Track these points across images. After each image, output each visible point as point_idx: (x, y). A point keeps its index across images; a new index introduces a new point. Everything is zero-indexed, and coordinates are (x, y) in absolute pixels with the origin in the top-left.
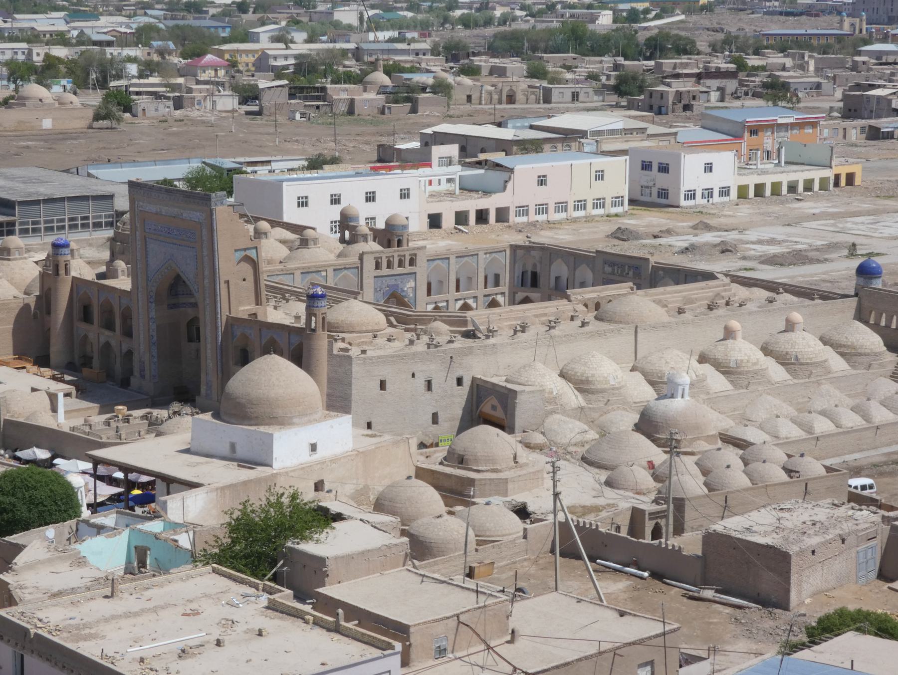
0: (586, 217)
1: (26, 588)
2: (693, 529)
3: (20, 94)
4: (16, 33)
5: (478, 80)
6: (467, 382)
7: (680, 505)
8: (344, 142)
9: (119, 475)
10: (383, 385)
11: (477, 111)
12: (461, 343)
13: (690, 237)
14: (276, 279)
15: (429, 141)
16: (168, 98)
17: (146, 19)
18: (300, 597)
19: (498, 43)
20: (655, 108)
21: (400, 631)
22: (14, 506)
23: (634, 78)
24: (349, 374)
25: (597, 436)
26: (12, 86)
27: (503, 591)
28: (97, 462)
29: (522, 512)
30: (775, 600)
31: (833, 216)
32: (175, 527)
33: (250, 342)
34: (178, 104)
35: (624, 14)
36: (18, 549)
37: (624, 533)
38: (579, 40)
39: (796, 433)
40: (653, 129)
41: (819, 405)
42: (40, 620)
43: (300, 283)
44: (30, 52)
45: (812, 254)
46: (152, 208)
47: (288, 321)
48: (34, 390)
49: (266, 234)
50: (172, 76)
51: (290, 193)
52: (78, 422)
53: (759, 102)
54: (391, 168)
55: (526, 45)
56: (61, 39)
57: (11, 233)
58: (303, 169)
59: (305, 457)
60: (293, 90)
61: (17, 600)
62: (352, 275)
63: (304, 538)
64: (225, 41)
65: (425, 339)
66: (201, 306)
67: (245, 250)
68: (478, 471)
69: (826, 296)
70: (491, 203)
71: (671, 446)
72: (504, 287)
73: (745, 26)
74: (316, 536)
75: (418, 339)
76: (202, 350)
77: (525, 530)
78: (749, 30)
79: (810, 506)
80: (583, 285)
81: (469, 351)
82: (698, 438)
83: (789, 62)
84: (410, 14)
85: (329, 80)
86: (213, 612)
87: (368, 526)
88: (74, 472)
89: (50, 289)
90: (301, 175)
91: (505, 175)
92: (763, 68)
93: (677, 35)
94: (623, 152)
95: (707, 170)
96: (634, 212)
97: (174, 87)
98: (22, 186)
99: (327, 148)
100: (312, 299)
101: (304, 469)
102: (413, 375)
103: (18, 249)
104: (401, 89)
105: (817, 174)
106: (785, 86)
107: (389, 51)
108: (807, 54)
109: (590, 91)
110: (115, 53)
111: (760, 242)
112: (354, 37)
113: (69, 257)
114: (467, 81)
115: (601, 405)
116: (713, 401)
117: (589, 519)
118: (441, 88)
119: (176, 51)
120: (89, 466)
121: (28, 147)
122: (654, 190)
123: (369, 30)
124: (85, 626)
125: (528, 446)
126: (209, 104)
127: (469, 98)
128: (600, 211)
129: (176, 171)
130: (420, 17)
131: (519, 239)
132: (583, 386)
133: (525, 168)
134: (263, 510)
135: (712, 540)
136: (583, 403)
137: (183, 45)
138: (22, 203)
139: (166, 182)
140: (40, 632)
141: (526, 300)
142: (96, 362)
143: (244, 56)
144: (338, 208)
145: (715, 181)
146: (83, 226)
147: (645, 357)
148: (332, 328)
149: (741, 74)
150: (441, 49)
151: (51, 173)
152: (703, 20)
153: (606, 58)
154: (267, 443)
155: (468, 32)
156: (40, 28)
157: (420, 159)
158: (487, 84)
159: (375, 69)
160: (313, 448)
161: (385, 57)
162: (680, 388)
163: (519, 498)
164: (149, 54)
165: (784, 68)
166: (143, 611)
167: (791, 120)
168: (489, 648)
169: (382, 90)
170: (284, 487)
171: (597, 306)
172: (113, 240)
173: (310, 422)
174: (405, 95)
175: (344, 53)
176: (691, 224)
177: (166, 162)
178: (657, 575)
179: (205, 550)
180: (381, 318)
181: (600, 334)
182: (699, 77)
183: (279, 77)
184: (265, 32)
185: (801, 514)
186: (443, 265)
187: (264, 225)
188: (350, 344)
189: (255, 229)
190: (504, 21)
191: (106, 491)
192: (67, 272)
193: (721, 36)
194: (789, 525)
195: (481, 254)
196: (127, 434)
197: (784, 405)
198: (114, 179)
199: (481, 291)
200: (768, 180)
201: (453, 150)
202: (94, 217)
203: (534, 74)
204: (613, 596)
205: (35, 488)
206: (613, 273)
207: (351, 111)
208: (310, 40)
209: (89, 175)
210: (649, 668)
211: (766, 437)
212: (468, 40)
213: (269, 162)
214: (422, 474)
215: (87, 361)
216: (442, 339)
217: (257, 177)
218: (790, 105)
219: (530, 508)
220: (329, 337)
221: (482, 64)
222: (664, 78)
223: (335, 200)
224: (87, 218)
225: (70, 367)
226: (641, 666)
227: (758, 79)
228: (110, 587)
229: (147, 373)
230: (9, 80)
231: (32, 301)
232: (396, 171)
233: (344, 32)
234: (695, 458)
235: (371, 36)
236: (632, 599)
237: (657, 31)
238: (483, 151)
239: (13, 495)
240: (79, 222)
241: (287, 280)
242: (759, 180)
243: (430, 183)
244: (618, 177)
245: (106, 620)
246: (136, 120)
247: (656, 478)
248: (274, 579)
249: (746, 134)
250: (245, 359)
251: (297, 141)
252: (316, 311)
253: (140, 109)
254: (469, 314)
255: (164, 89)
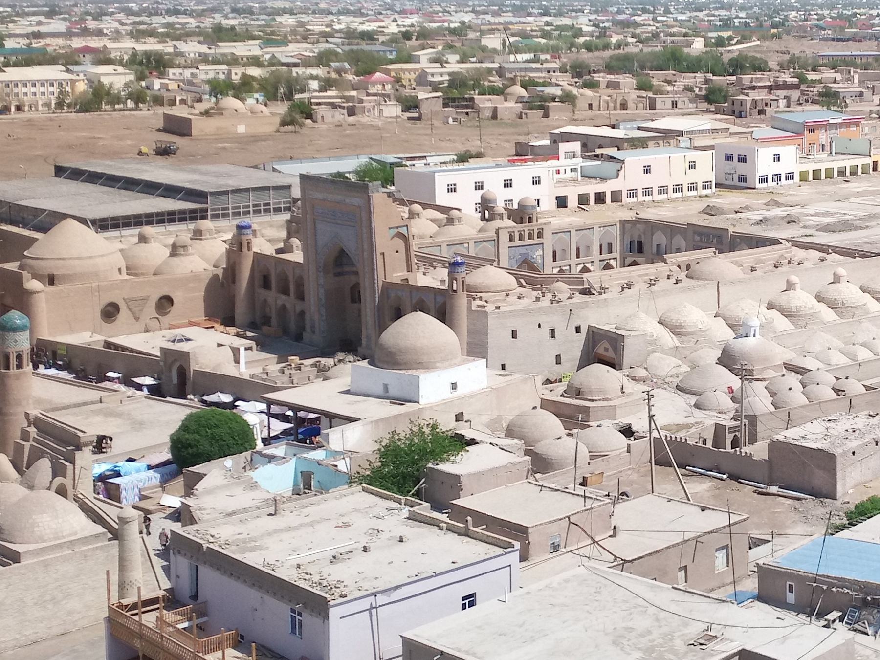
0: (683, 197)
1: (205, 509)
2: (763, 439)
3: (219, 105)
4: (219, 57)
5: (598, 92)
6: (584, 330)
7: (753, 420)
8: (488, 141)
9: (290, 413)
10: (514, 334)
11: (596, 116)
12: (578, 298)
13: (764, 212)
14: (426, 251)
15: (558, 139)
16: (343, 108)
17: (327, 45)
18: (437, 507)
19: (614, 63)
20: (737, 113)
21: (520, 532)
22: (198, 442)
23: (720, 90)
24: (486, 326)
25: (689, 369)
26: (213, 99)
27: (609, 495)
28: (270, 403)
29: (627, 432)
30: (825, 492)
31: (872, 193)
32: (336, 454)
33: (401, 302)
34: (351, 112)
35: (713, 40)
36: (200, 477)
37: (709, 445)
38: (675, 61)
39: (844, 360)
40: (734, 129)
41: (861, 338)
42: (213, 536)
43: (446, 253)
44: (230, 72)
45: (858, 223)
46: (319, 196)
47: (435, 284)
48: (219, 345)
49: (418, 214)
50: (347, 90)
51: (441, 181)
52: (257, 370)
53: (817, 107)
54: (526, 161)
55: (636, 64)
56: (255, 62)
57: (204, 217)
58: (453, 162)
59: (446, 393)
60: (447, 101)
61: (197, 520)
62: (490, 246)
63: (442, 460)
64: (392, 62)
65: (549, 296)
66: (361, 274)
67: (397, 228)
68: (593, 401)
69: (865, 255)
70: (607, 188)
71: (745, 374)
72: (617, 254)
73: (806, 50)
74: (452, 458)
75: (543, 296)
76: (363, 309)
77: (629, 445)
78: (809, 53)
79: (851, 417)
80: (678, 251)
81: (586, 305)
82: (768, 368)
83: (839, 77)
84: (543, 41)
85: (477, 92)
86: (362, 523)
87: (497, 448)
88: (251, 413)
89: (234, 263)
90: (450, 167)
91: (618, 166)
92: (820, 81)
93: (753, 57)
94: (712, 147)
95: (775, 158)
96: (721, 193)
97: (348, 99)
98: (214, 179)
99: (474, 145)
100: (453, 266)
101: (446, 404)
102: (539, 325)
103: (209, 231)
104: (536, 99)
105: (860, 162)
106: (836, 95)
107: (526, 70)
108: (852, 70)
109: (686, 99)
110: (300, 73)
111: (817, 215)
112: (498, 58)
113: (251, 236)
114: (588, 92)
115: (692, 344)
116: (779, 338)
117: (682, 434)
118: (568, 98)
119: (351, 70)
120: (263, 406)
121: (224, 148)
122: (735, 176)
123: (510, 53)
124: (252, 540)
125: (634, 379)
126: (377, 112)
127: (590, 106)
128: (694, 193)
129: (349, 165)
130: (551, 42)
131: (629, 215)
132: (677, 330)
133: (633, 159)
134: (407, 439)
135: (775, 447)
136: (678, 344)
137: (357, 65)
138: (212, 194)
139: (340, 175)
140: (211, 546)
141: (634, 264)
142: (274, 321)
143: (407, 73)
144: (480, 192)
145: (782, 168)
146: (265, 210)
147: (726, 306)
148: (472, 291)
149: (802, 86)
150: (568, 68)
151: (237, 168)
152: (774, 45)
153: (698, 75)
154: (415, 384)
155: (590, 54)
156: (238, 53)
157: (551, 153)
158: (604, 94)
159: (515, 84)
160: (454, 386)
161: (523, 74)
162: (752, 329)
163: (625, 421)
164: (328, 73)
165: (835, 82)
166: (301, 525)
167: (840, 121)
168: (594, 542)
169: (520, 100)
170: (426, 419)
171: (688, 267)
172: (289, 222)
173: (451, 366)
174: (539, 104)
175: (489, 71)
176: (764, 202)
177: (339, 158)
178: (734, 477)
179: (358, 473)
180: (513, 279)
181: (689, 289)
182: (770, 88)
183: (435, 90)
184: (424, 55)
185: (845, 423)
186: (565, 236)
187: (417, 208)
188: (486, 302)
189: (409, 210)
190: (618, 46)
191: (278, 427)
192: (249, 249)
193: (787, 57)
194: (835, 432)
195: (596, 228)
196: (298, 379)
197: (834, 339)
198: (290, 172)
199: (597, 257)
200: (823, 167)
201: (576, 146)
202: (274, 204)
203: (641, 87)
204: (699, 495)
205: (216, 426)
206: (701, 241)
207: (494, 116)
208: (462, 61)
209: (274, 170)
210: (724, 551)
211: (821, 365)
212: (590, 61)
213: (425, 157)
214: (546, 405)
215: (267, 321)
216: (563, 296)
217: (414, 169)
218: (840, 109)
219: (634, 429)
220: (468, 296)
221: (601, 79)
222: (744, 90)
223: (479, 186)
224: (269, 204)
225: (253, 326)
226: (718, 550)
227: (815, 90)
228: (275, 506)
229: (317, 330)
230: (210, 96)
231: (220, 272)
232: (529, 163)
233: (490, 54)
234: (765, 383)
235: (512, 58)
236: (715, 497)
237: (737, 53)
238: (600, 147)
239: (198, 433)
240: (262, 208)
241: (435, 251)
242: (816, 167)
243: (558, 172)
244: (706, 168)
245: (269, 534)
246: (316, 125)
247: (733, 399)
248: (418, 494)
249: (806, 132)
250: (398, 314)
251: (449, 140)
252: (456, 275)
253: (319, 117)
254: (585, 275)
255: (339, 100)
